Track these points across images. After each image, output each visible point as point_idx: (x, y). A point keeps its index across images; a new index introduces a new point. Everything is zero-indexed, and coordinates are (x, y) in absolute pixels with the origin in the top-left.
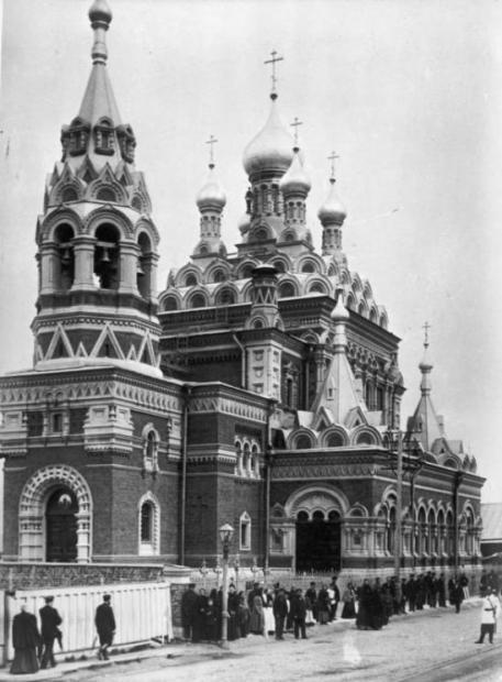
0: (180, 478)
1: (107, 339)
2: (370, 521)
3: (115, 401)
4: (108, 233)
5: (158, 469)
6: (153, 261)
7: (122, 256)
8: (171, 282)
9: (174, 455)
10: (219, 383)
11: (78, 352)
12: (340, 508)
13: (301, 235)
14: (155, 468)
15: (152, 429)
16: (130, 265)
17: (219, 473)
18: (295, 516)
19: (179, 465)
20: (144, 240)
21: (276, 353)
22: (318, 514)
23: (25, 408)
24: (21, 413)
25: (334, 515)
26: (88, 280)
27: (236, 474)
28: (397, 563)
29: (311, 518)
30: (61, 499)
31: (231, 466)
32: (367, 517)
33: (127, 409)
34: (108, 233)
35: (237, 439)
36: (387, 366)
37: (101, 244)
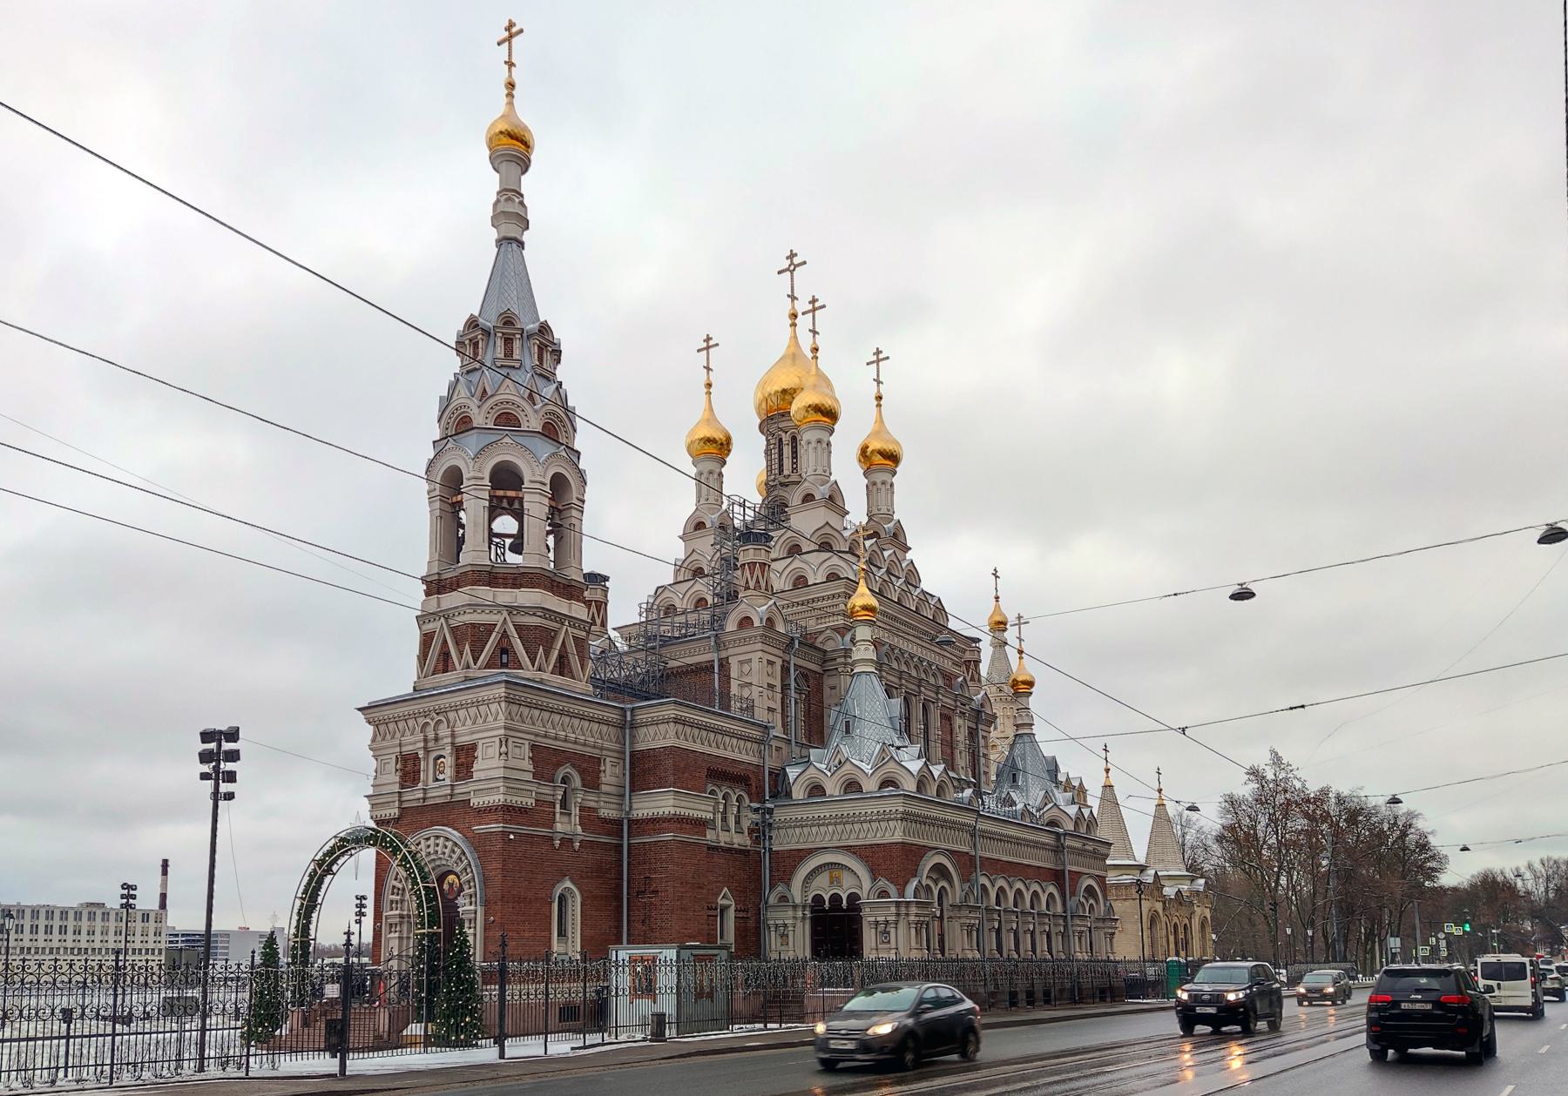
22: (836, 898)
23: (532, 737)
25: (853, 898)
33: (527, 742)
37: (500, 493)
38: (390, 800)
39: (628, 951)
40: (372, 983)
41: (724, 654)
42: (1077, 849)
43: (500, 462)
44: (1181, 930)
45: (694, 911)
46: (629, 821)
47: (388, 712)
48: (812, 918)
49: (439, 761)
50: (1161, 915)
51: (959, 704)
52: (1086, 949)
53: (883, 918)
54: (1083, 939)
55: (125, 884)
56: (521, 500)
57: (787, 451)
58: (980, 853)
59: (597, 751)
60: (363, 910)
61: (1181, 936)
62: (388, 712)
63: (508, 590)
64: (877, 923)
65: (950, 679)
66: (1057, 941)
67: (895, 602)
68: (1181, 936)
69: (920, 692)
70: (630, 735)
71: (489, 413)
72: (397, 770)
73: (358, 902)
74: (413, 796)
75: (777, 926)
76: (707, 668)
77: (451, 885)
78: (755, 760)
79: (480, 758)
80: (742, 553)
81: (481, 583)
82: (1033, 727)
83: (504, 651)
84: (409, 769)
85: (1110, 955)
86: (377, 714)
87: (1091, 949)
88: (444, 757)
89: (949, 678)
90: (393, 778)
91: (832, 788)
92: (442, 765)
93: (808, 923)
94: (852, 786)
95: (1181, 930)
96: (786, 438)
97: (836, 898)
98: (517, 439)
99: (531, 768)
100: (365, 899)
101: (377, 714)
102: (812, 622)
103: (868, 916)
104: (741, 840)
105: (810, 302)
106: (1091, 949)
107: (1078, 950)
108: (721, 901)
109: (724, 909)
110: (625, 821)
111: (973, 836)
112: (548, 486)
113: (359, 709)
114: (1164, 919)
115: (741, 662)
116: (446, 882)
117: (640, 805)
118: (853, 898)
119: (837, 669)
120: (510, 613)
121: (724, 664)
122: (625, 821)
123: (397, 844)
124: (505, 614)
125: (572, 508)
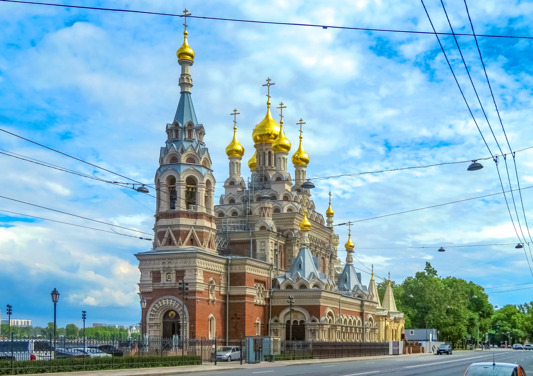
0: (225, 304)
1: (192, 234)
2: (319, 325)
3: (197, 268)
4: (191, 181)
5: (215, 299)
6: (212, 193)
7: (199, 191)
8: (222, 201)
9: (222, 292)
10: (247, 257)
11: (179, 243)
12: (305, 318)
13: (285, 176)
14: (214, 298)
15: (212, 279)
16: (202, 193)
17: (197, 284)
18: (286, 323)
19: (225, 297)
20: (208, 182)
21: (272, 242)
22: (295, 322)
23: (151, 270)
24: (149, 272)
25: (302, 322)
26: (182, 205)
27: (255, 301)
28: (190, 128)
29: (299, 324)
30: (170, 315)
31: (252, 297)
32: (318, 323)
33: (202, 271)
34: (191, 181)
35: (255, 285)
36: (327, 245)
37: (189, 186)
38: (149, 286)
39: (252, 338)
40: (149, 343)
41: (254, 238)
42: (368, 305)
43: (193, 176)
44: (394, 331)
45: (251, 325)
46: (229, 296)
47: (144, 258)
48: (286, 328)
49: (168, 275)
50: (389, 326)
51: (327, 253)
52: (327, 337)
53: (314, 329)
54: (326, 333)
55: (8, 305)
56: (196, 188)
57: (267, 157)
58: (341, 308)
59: (219, 273)
60: (11, 312)
61: (394, 333)
62: (144, 258)
63: (192, 219)
64: (311, 330)
65: (324, 244)
66: (360, 336)
67: (314, 221)
68: (394, 333)
69: (316, 250)
70: (230, 268)
71: (168, 157)
72: (151, 276)
73: (83, 313)
74: (157, 286)
75: (274, 330)
76: (248, 242)
77: (172, 315)
78: (267, 276)
79: (187, 275)
80: (262, 203)
81: (184, 217)
82: (352, 262)
83: (191, 240)
84: (156, 276)
85: (366, 340)
86: (142, 258)
87: (329, 337)
88: (171, 274)
89: (324, 244)
90: (149, 279)
91: (296, 286)
92: (169, 276)
93: (285, 329)
94: (303, 286)
95: (394, 331)
96: (267, 152)
97: (295, 322)
98: (195, 168)
99: (203, 279)
100: (86, 312)
101: (142, 258)
102: (282, 226)
103: (308, 328)
104: (263, 302)
105: (267, 80)
106: (329, 337)
107: (324, 337)
108: (257, 322)
109: (258, 324)
110: (228, 296)
111: (339, 302)
112: (205, 184)
113: (135, 255)
114: (390, 328)
115: (261, 242)
116: (170, 313)
117: (233, 291)
118: (302, 322)
119: (291, 244)
120: (194, 227)
121: (254, 242)
122: (228, 296)
123: (383, 333)
124: (193, 228)
125: (211, 191)
